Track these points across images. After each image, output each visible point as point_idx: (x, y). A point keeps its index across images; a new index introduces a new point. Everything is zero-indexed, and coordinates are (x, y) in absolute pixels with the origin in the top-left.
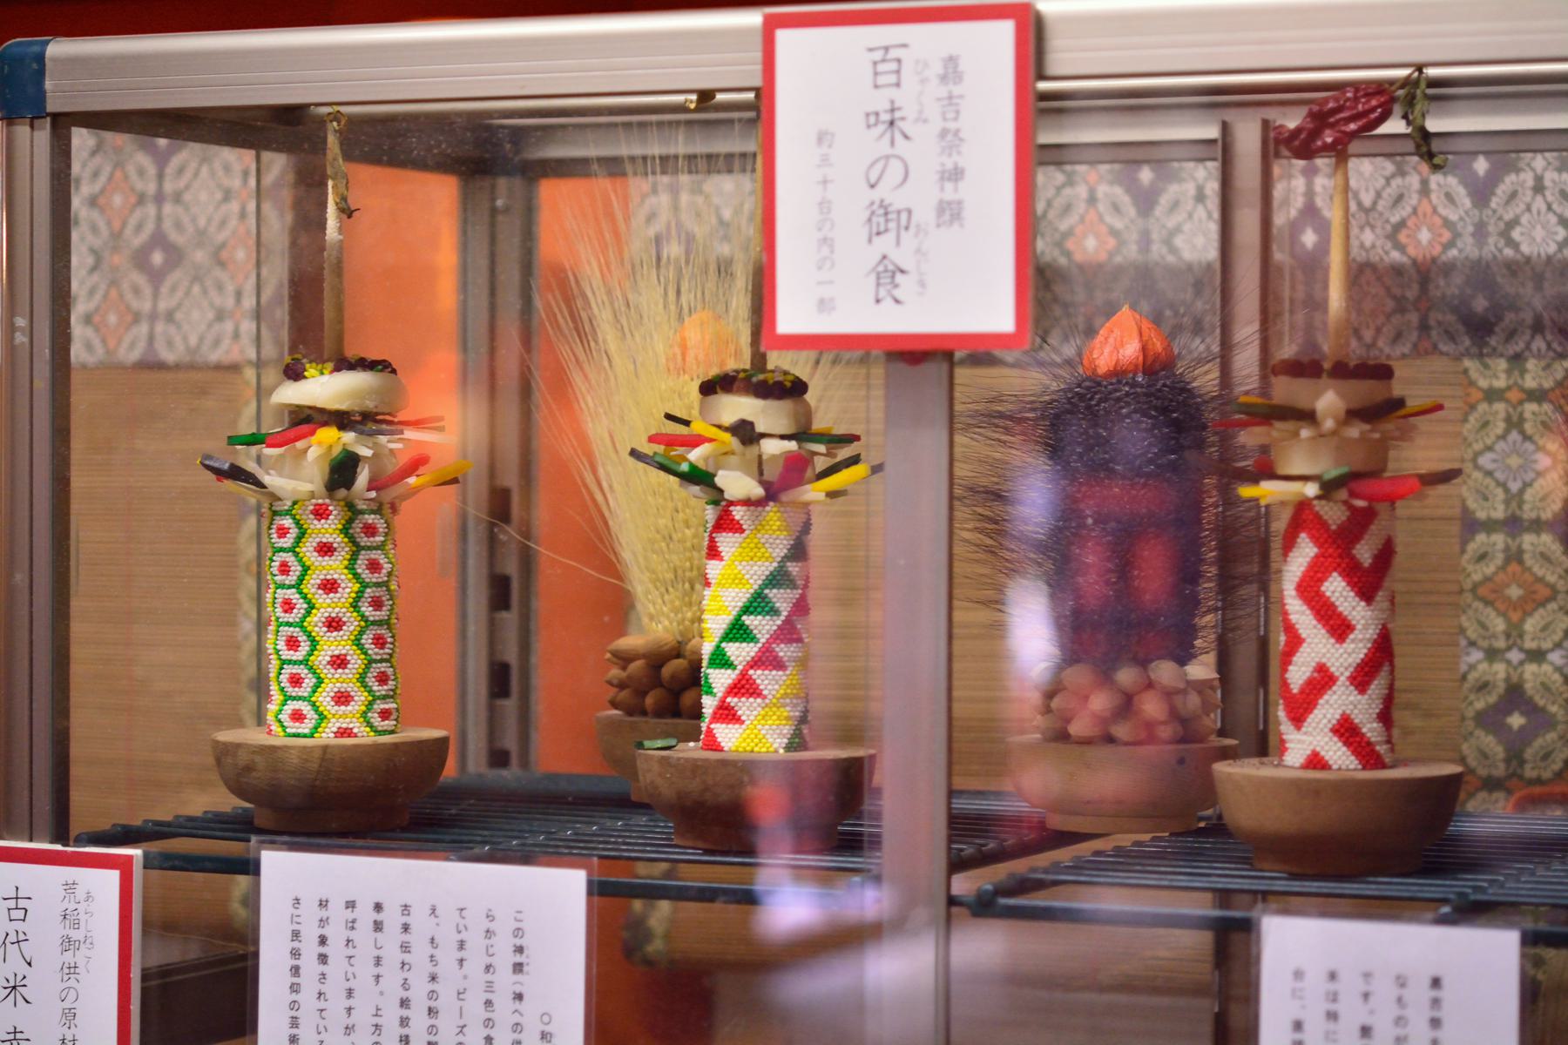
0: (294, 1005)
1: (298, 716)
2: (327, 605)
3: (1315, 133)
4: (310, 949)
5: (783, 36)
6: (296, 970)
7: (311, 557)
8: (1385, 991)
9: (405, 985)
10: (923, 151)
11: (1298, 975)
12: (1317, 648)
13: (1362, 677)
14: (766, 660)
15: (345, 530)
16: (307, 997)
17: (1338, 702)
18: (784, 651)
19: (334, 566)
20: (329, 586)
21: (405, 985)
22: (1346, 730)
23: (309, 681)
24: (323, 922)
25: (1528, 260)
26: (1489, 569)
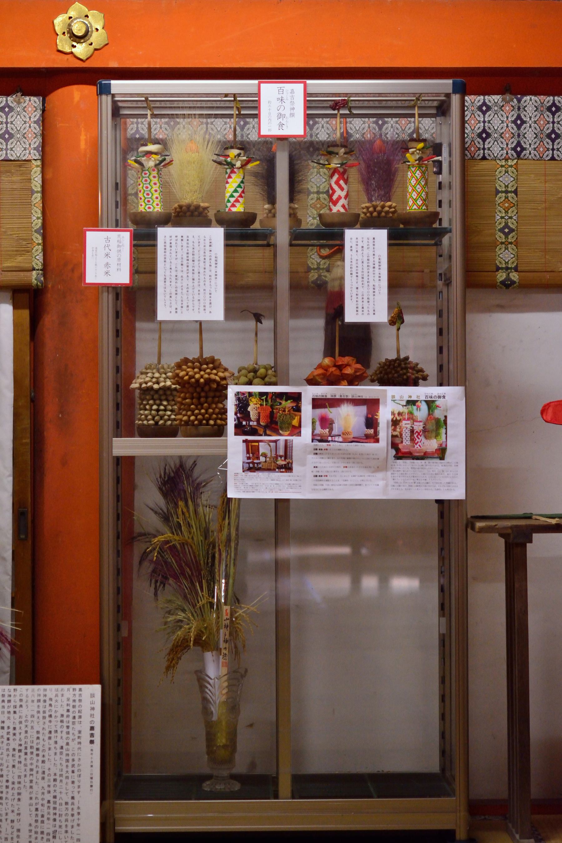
0: (165, 255)
1: (149, 208)
2: (155, 187)
3: (336, 107)
4: (168, 245)
5: (262, 85)
6: (165, 249)
7: (152, 178)
8: (365, 240)
9: (188, 250)
10: (287, 105)
11: (351, 239)
12: (339, 192)
13: (346, 197)
14: (241, 196)
15: (158, 174)
16: (168, 254)
17: (342, 201)
18: (243, 195)
19: (156, 180)
20: (155, 184)
21: (188, 250)
22: (343, 206)
23: (151, 201)
24: (171, 240)
25: (321, 141)
26: (314, 201)
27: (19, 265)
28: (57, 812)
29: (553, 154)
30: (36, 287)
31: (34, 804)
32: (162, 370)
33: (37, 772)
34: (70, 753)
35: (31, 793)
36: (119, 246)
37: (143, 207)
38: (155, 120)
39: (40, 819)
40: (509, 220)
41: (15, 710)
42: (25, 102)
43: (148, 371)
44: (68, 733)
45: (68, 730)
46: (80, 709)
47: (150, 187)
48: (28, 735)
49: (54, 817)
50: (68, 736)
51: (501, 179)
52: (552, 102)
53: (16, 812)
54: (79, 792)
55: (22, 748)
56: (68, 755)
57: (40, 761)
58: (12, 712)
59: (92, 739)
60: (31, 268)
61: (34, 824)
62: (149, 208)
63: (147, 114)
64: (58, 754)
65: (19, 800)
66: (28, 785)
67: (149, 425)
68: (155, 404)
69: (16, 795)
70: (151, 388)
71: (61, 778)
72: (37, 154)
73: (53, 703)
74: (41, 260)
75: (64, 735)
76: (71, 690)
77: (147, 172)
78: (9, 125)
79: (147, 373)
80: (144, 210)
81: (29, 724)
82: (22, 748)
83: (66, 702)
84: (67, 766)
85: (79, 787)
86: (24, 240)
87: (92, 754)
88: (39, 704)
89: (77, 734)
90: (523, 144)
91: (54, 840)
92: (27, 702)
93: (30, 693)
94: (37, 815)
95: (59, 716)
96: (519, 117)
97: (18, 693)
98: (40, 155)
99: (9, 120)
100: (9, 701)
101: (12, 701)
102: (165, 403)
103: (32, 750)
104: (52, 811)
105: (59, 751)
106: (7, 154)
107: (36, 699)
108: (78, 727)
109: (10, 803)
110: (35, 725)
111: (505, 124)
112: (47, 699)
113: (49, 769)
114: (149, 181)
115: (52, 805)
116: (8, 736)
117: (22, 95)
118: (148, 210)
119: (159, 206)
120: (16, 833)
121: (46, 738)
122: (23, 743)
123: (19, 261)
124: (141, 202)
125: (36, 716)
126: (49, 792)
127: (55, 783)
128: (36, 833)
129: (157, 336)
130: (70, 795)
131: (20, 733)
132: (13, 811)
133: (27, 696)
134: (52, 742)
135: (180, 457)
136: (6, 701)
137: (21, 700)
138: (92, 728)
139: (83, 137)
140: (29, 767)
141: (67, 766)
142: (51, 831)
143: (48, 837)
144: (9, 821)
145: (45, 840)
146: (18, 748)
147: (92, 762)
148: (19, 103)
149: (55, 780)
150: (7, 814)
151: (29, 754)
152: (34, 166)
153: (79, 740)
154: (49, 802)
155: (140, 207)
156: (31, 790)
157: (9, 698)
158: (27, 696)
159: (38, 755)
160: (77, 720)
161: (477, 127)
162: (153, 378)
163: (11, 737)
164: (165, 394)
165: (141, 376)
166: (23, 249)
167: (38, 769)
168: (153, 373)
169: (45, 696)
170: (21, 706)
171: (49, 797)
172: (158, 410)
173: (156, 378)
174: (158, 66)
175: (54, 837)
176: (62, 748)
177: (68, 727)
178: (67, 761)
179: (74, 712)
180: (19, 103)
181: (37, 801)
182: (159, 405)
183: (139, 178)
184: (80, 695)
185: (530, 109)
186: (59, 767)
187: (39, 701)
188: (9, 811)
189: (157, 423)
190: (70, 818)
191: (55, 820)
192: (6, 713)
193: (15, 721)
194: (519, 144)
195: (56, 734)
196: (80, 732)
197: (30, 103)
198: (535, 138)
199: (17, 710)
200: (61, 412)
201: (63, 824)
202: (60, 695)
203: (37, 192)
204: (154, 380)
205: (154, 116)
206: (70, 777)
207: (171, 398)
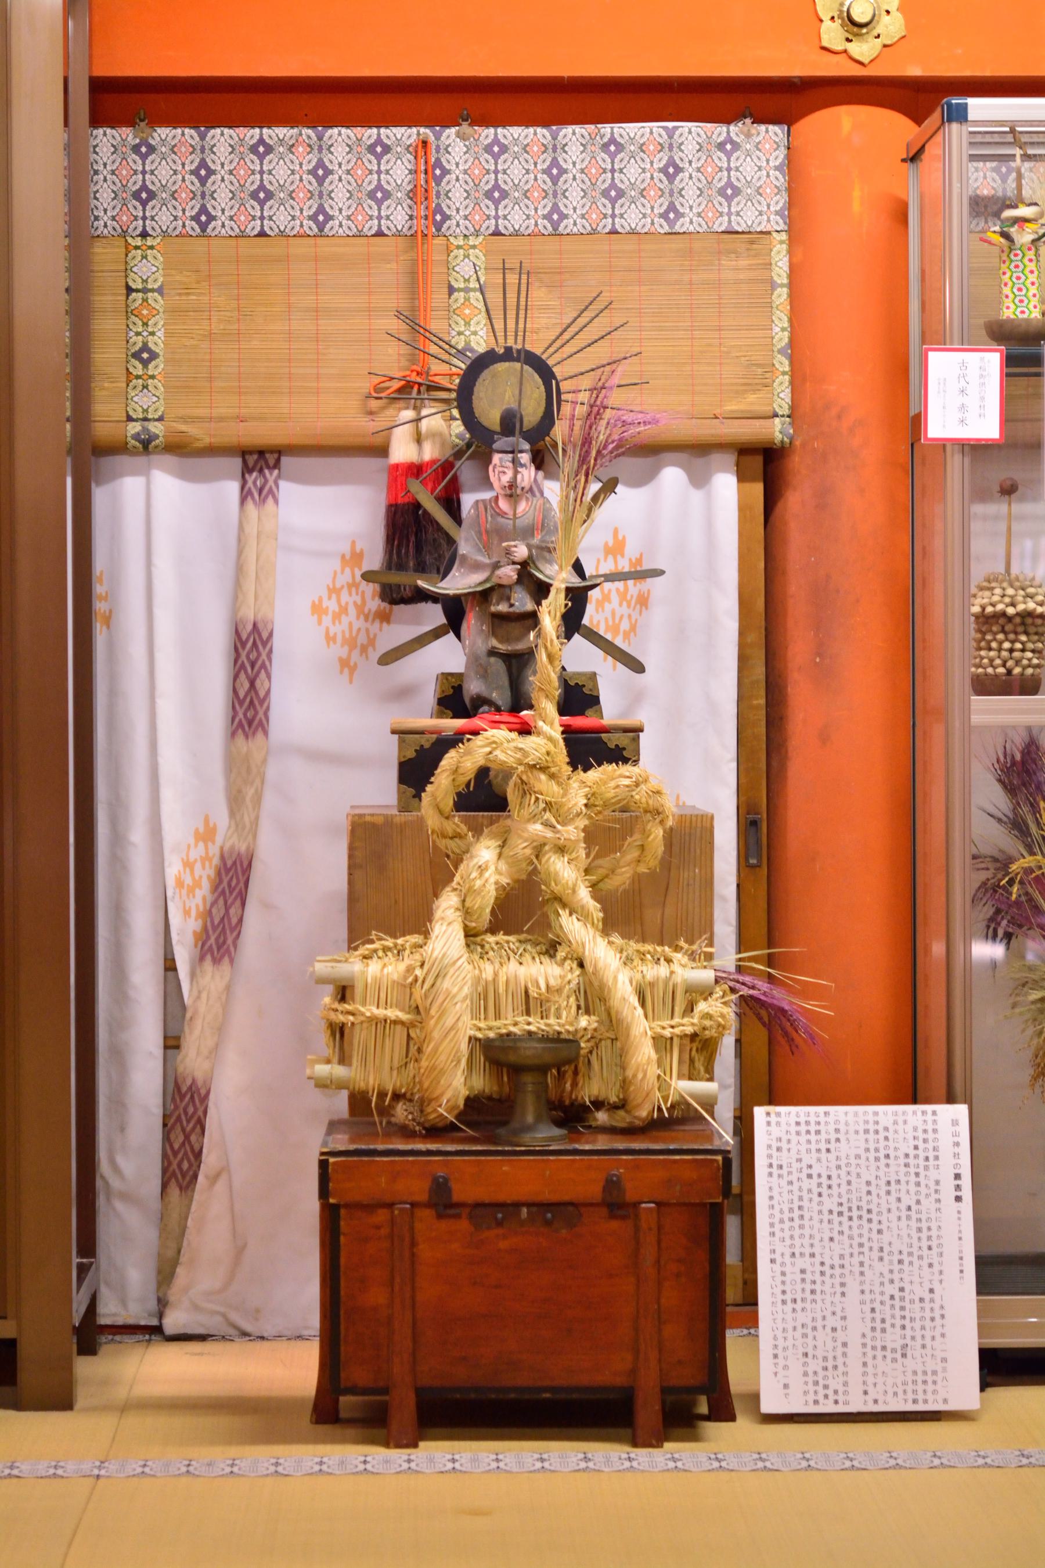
1: (1023, 312)
2: (1032, 278)
20: (1032, 272)
23: (1026, 301)
27: (748, 408)
28: (907, 1313)
29: (144, 226)
30: (779, 445)
31: (868, 1302)
32: (1017, 584)
33: (871, 1249)
34: (924, 1217)
35: (862, 1283)
36: (982, 376)
37: (1011, 310)
38: (975, 164)
39: (878, 1325)
40: (473, 337)
41: (828, 1146)
42: (759, 134)
43: (993, 585)
44: (918, 1184)
45: (918, 1179)
46: (935, 1144)
47: (1023, 277)
48: (853, 1187)
49: (903, 1322)
50: (919, 1189)
51: (155, 269)
52: (375, 137)
53: (839, 1314)
54: (941, 1281)
55: (844, 1209)
56: (919, 1220)
57: (875, 1231)
58: (824, 1151)
59: (959, 1194)
60: (771, 414)
61: (869, 1334)
62: (1023, 312)
63: (1014, 155)
64: (904, 1218)
65: (843, 1294)
66: (857, 1269)
67: (997, 676)
68: (1007, 640)
69: (838, 1286)
70: (1004, 614)
71: (911, 1259)
72: (781, 221)
73: (890, 1135)
74: (788, 400)
75: (913, 1188)
76: (919, 1114)
77: (1019, 252)
78: (732, 173)
79: (992, 589)
80: (1013, 317)
81: (852, 1169)
82: (844, 1209)
83: (911, 1134)
84: (919, 1239)
85: (941, 1272)
86: (759, 365)
87: (959, 1219)
88: (867, 1136)
89: (933, 1187)
90: (328, 209)
91: (904, 1360)
92: (847, 1133)
93: (850, 1118)
94: (873, 1319)
95: (902, 1156)
96: (203, 164)
97: (831, 1119)
98: (785, 223)
99: (147, 168)
100: (818, 1132)
101: (823, 1132)
102: (1024, 638)
103: (860, 1213)
104: (898, 1313)
105: (904, 1214)
106: (730, 222)
107: (861, 1128)
108: (933, 1174)
109: (828, 1299)
110: (863, 1171)
111: (180, 177)
112: (880, 1128)
113: (890, 1244)
114: (1021, 266)
115: (897, 1303)
116: (820, 1190)
117: (753, 123)
118: (1021, 316)
119: (1037, 310)
120: (840, 1350)
121: (883, 1193)
122: (844, 1200)
123: (752, 402)
124: (1008, 302)
125: (864, 1156)
126: (892, 1281)
127: (900, 1266)
128: (874, 1348)
129: (1003, 527)
130: (927, 1286)
131: (839, 1185)
132: (834, 1313)
133: (847, 1124)
134: (892, 1199)
135: (1029, 729)
136: (813, 1132)
137: (837, 1131)
138: (957, 1176)
139: (856, 194)
140: (857, 1240)
141: (919, 1239)
142: (898, 1345)
143: (894, 1355)
144: (828, 1329)
145: (889, 1359)
146: (836, 1209)
147: (960, 1232)
148: (748, 135)
149: (900, 1262)
150: (824, 1318)
151: (855, 1218)
152: (775, 242)
153: (937, 1196)
154: (892, 1297)
155: (1005, 310)
156: (863, 1278)
157: (818, 1128)
158: (847, 1124)
159: (870, 1221)
160: (932, 1162)
161: (249, 181)
162: (1003, 596)
163: (824, 1190)
164: (1023, 624)
165: (981, 593)
166: (757, 381)
167: (871, 1244)
168: (1004, 589)
169: (877, 1123)
170: (838, 1140)
171: (890, 1289)
172: (1011, 651)
173: (1010, 596)
174: (988, 73)
175: (904, 1355)
176: (909, 1208)
177: (917, 1174)
178: (920, 1230)
179: (926, 1150)
180: (748, 135)
181: (873, 1296)
182: (1013, 642)
183: (1004, 262)
184: (935, 1121)
185: (690, 147)
186: (906, 1240)
187: (866, 1131)
188: (828, 1314)
189: (1009, 672)
190: (928, 1323)
191: (903, 1327)
192: (813, 1151)
193: (830, 1165)
194: (321, 210)
195: (898, 1187)
196: (937, 1183)
197: (767, 136)
198: (465, 199)
199: (832, 1146)
200: (819, 654)
201: (918, 1334)
202: (900, 1122)
203: (782, 286)
204: (1007, 600)
205: (1026, 157)
206: (925, 1257)
207: (1032, 630)
